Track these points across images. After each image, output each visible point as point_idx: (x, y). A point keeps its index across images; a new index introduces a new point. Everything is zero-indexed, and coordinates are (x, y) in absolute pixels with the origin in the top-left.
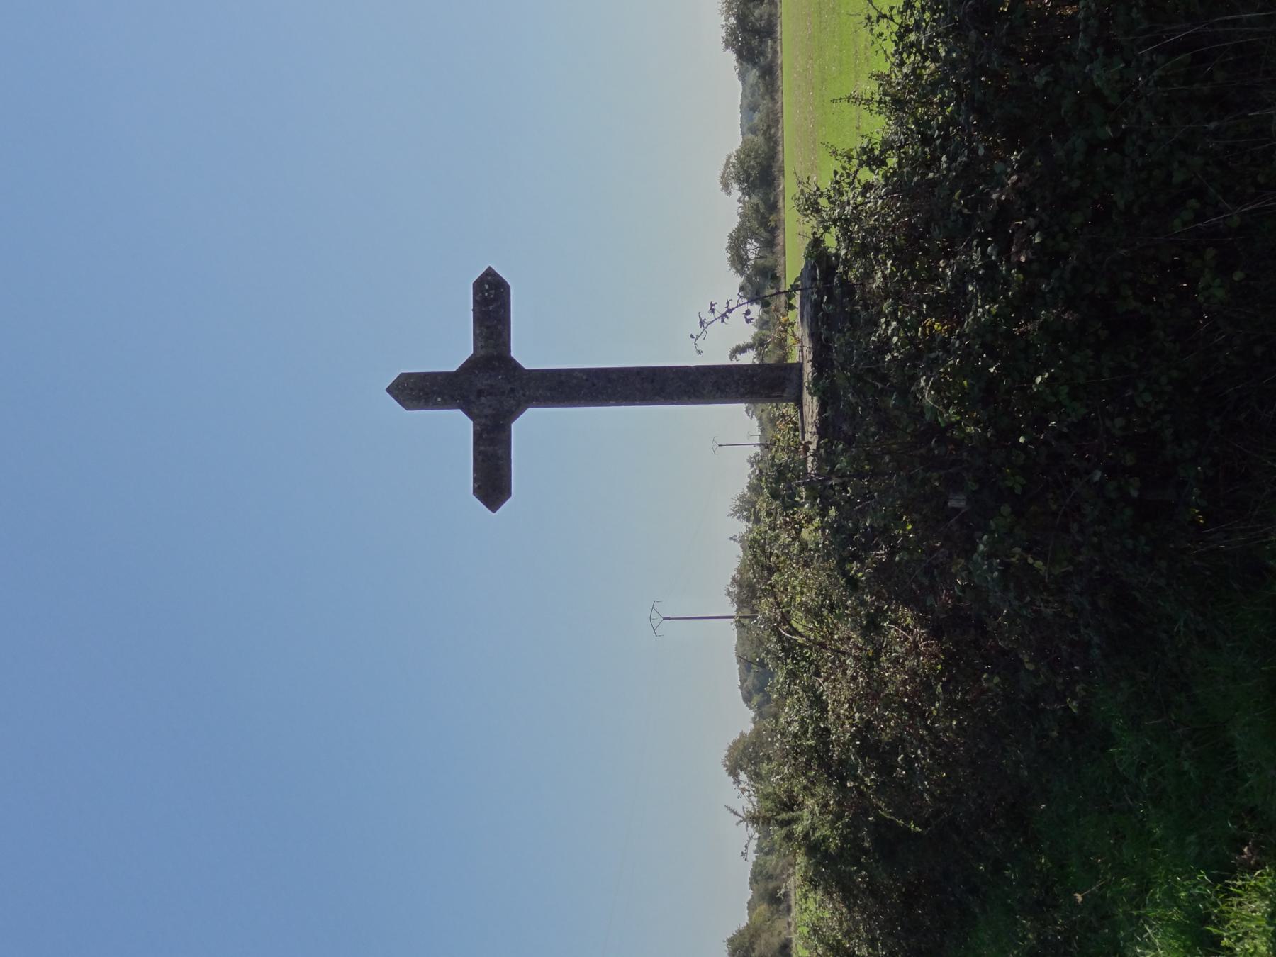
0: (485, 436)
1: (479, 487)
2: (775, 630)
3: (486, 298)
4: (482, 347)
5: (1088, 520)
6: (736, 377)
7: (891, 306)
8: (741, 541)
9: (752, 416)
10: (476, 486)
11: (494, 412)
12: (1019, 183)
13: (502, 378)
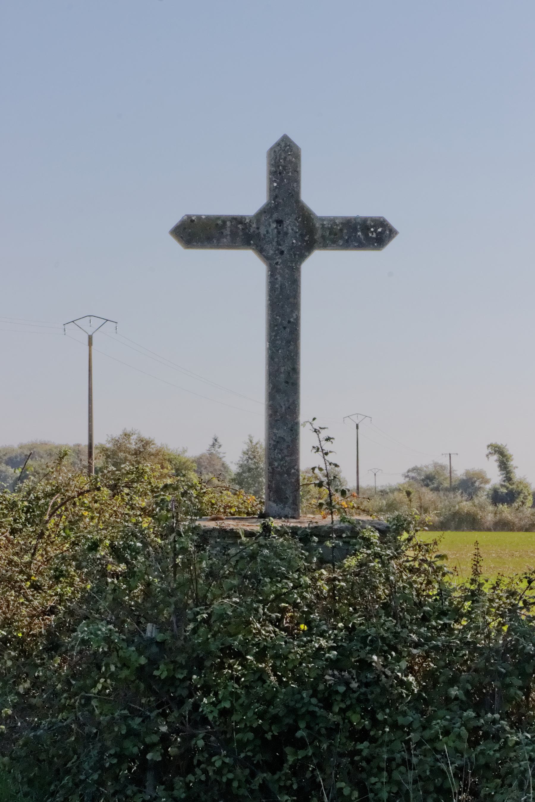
0: (240, 226)
1: (192, 221)
2: (57, 490)
3: (369, 229)
4: (323, 225)
5: (130, 722)
6: (288, 459)
7: (305, 582)
8: (211, 454)
9: (407, 476)
10: (193, 218)
11: (262, 236)
12: (384, 676)
13: (293, 243)
